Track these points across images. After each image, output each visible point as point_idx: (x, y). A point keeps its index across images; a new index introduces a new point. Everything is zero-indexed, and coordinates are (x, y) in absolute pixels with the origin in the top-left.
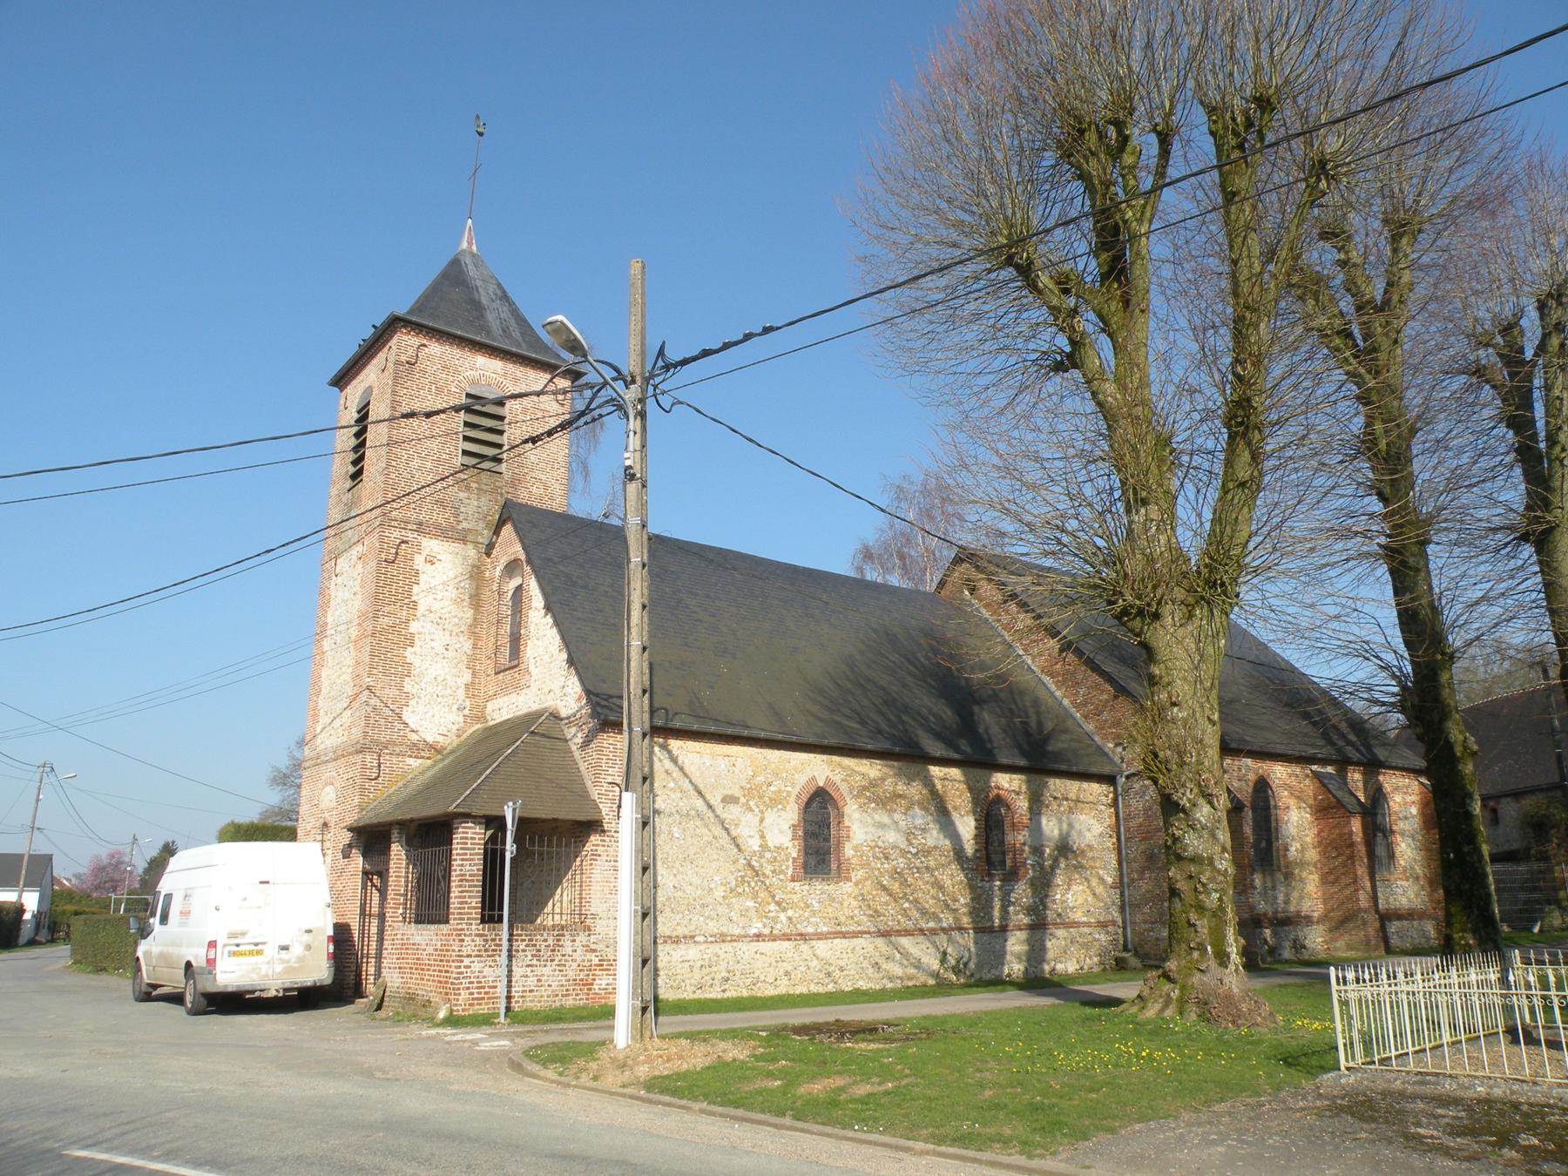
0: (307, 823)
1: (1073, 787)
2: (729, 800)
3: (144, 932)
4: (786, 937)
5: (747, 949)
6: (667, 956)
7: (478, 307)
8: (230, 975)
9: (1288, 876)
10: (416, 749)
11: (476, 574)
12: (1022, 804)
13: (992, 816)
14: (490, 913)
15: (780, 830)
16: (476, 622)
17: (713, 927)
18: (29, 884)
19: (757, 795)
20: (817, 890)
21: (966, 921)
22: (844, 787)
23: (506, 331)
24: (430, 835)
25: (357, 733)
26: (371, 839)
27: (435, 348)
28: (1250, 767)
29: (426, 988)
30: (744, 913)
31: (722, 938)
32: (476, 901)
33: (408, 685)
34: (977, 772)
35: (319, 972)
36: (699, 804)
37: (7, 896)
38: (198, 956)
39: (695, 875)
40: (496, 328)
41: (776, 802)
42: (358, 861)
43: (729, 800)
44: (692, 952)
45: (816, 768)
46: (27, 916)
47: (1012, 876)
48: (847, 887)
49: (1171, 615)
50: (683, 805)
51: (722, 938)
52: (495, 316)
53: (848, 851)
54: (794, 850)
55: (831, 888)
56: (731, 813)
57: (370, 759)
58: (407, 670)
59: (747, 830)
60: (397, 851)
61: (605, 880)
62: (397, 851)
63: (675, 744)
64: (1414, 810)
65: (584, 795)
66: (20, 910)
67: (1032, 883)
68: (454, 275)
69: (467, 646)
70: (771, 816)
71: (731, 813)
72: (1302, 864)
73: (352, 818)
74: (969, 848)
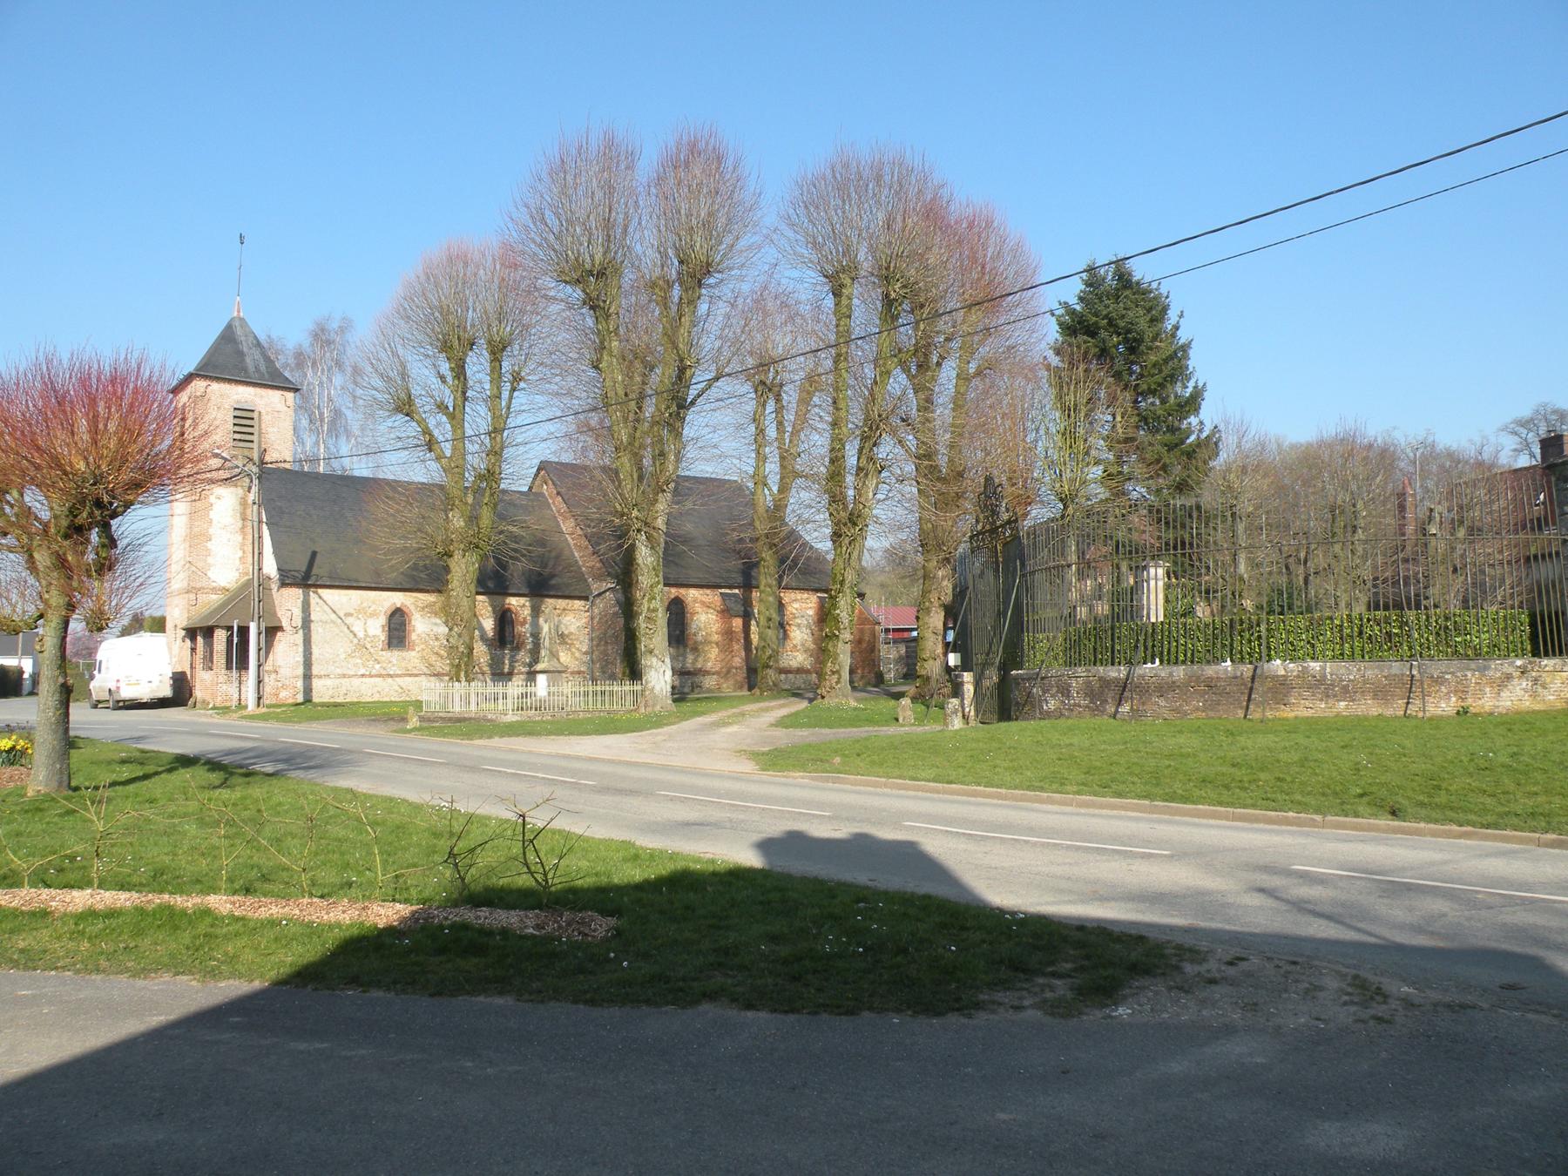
0: (169, 625)
1: (561, 603)
2: (348, 615)
3: (92, 677)
4: (380, 676)
5: (356, 682)
6: (316, 683)
7: (241, 354)
8: (127, 693)
9: (695, 649)
10: (214, 590)
11: (243, 503)
12: (527, 612)
13: (504, 620)
14: (229, 667)
15: (376, 628)
16: (244, 527)
17: (339, 671)
18: (25, 653)
19: (362, 612)
20: (395, 656)
21: (486, 669)
22: (412, 608)
23: (257, 369)
24: (208, 632)
25: (185, 584)
26: (191, 633)
27: (215, 386)
28: (674, 592)
29: (208, 698)
30: (355, 665)
31: (344, 676)
32: (224, 661)
33: (210, 560)
34: (499, 598)
35: (167, 692)
36: (333, 616)
37: (9, 662)
38: (113, 687)
39: (330, 648)
40: (251, 369)
41: (374, 615)
42: (188, 642)
43: (348, 615)
44: (328, 682)
45: (398, 599)
46: (26, 676)
47: (517, 648)
48: (413, 653)
49: (457, 556)
50: (325, 618)
51: (344, 676)
52: (252, 359)
53: (414, 637)
54: (383, 637)
55: (404, 654)
56: (349, 620)
57: (192, 596)
58: (208, 553)
59: (358, 627)
60: (200, 640)
61: (286, 652)
62: (200, 640)
63: (320, 591)
64: (811, 612)
65: (275, 614)
66: (21, 672)
67: (531, 651)
68: (228, 336)
69: (240, 538)
70: (370, 622)
71: (349, 620)
72: (707, 642)
73: (185, 624)
74: (490, 634)
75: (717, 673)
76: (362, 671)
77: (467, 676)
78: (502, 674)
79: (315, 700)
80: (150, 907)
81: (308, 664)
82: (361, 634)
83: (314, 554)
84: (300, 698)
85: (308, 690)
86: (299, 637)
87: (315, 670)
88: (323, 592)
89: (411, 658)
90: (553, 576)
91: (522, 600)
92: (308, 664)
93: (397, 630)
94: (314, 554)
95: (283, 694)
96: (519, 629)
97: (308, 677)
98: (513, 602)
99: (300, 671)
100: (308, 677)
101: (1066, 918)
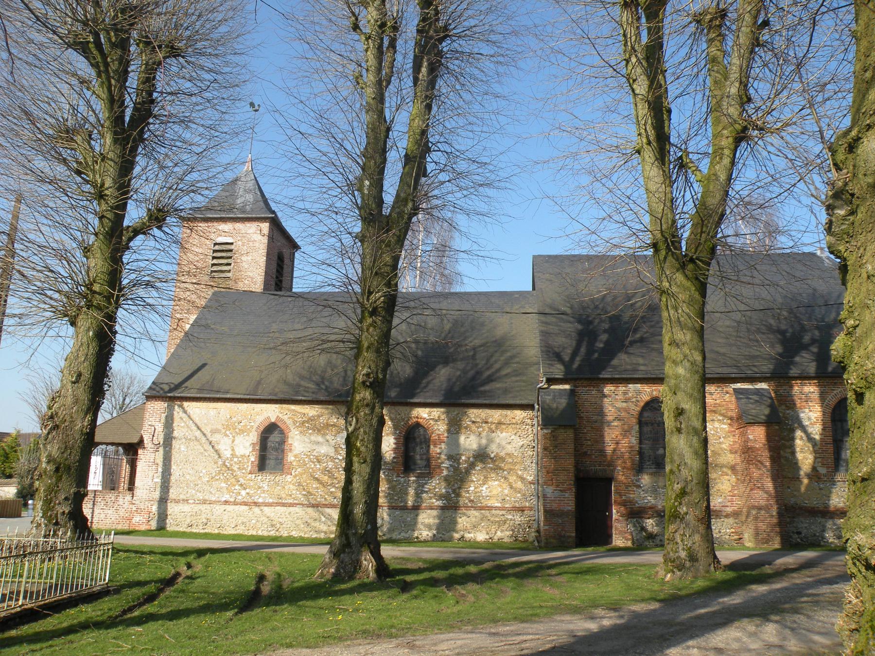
4: (245, 504)
5: (219, 509)
12: (441, 428)
15: (245, 446)
17: (200, 496)
19: (232, 428)
20: (265, 480)
22: (289, 422)
30: (219, 490)
31: (204, 502)
34: (402, 409)
36: (198, 433)
43: (214, 432)
44: (186, 508)
45: (271, 412)
47: (429, 470)
48: (289, 478)
51: (204, 502)
53: (290, 457)
59: (225, 447)
63: (186, 404)
70: (239, 439)
75: (736, 514)
76: (226, 497)
77: (788, 441)
78: (405, 508)
79: (170, 528)
80: (329, 577)
81: (165, 486)
82: (227, 454)
83: (204, 365)
84: (154, 525)
85: (162, 516)
86: (160, 456)
87: (173, 493)
88: (192, 407)
89: (286, 484)
90: (490, 380)
91: (437, 412)
92: (165, 486)
93: (270, 449)
94: (204, 365)
95: (137, 519)
96: (434, 450)
97: (163, 501)
98: (423, 414)
99: (157, 495)
100: (163, 501)
101: (267, 273)
